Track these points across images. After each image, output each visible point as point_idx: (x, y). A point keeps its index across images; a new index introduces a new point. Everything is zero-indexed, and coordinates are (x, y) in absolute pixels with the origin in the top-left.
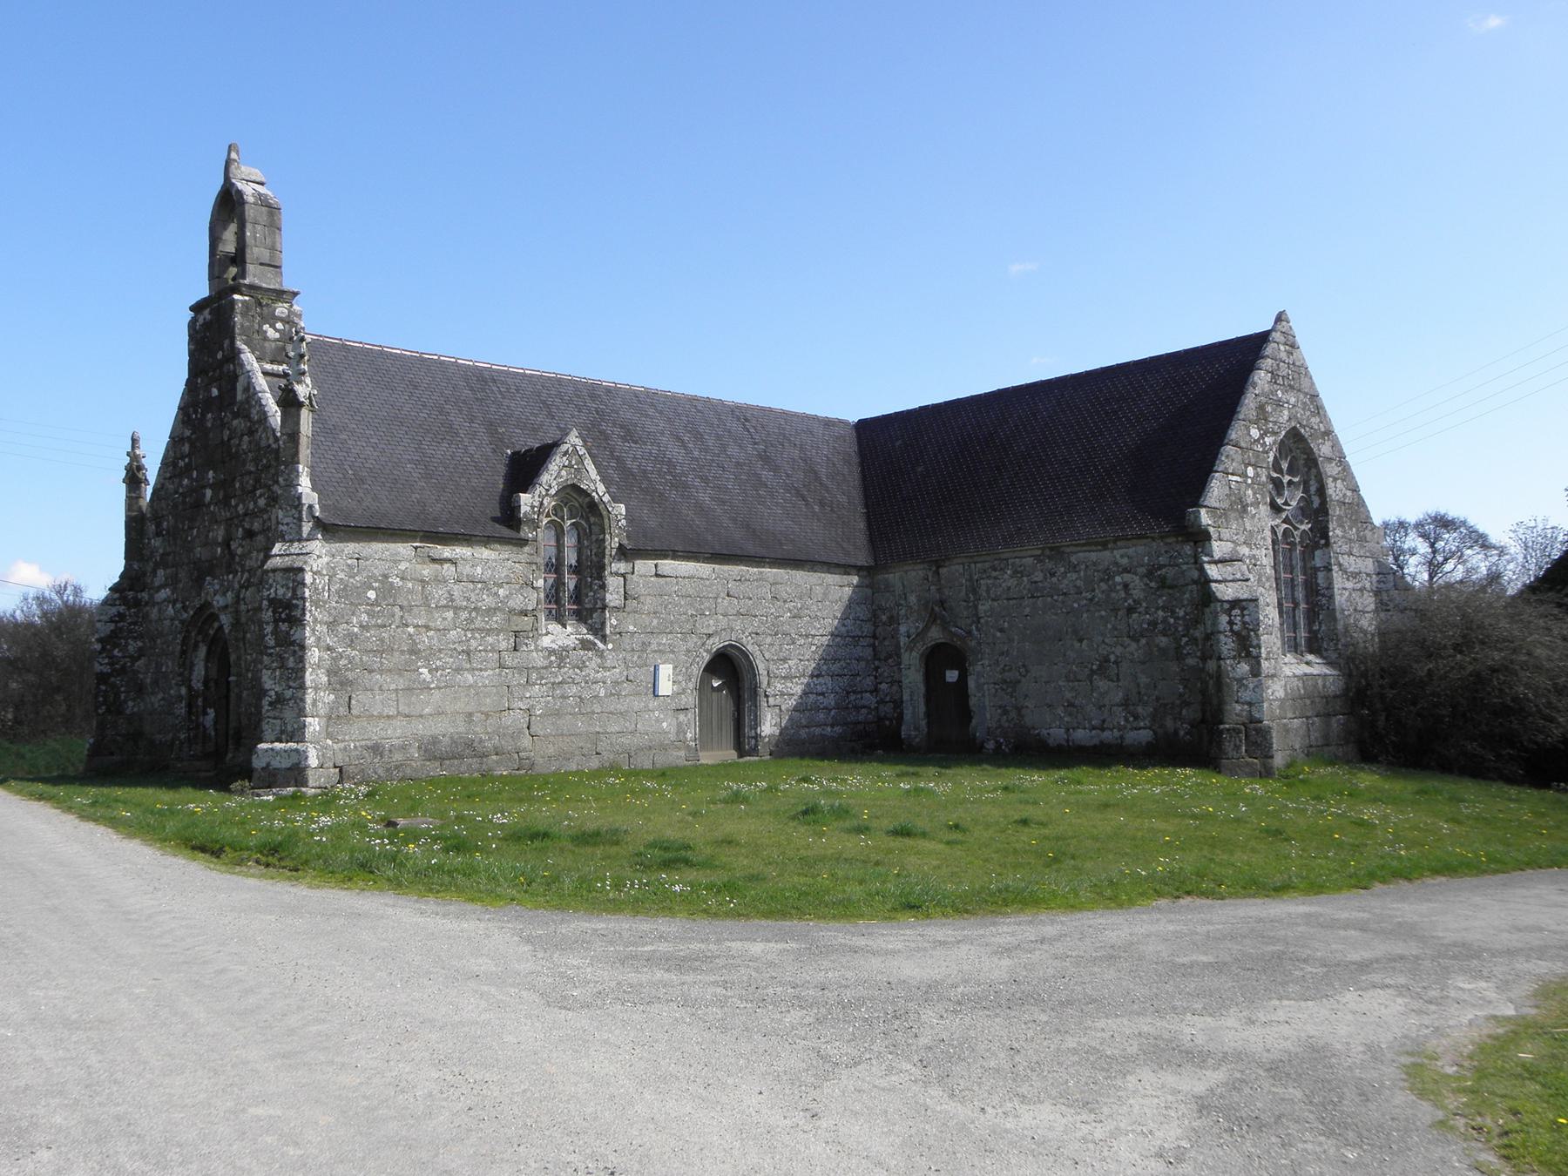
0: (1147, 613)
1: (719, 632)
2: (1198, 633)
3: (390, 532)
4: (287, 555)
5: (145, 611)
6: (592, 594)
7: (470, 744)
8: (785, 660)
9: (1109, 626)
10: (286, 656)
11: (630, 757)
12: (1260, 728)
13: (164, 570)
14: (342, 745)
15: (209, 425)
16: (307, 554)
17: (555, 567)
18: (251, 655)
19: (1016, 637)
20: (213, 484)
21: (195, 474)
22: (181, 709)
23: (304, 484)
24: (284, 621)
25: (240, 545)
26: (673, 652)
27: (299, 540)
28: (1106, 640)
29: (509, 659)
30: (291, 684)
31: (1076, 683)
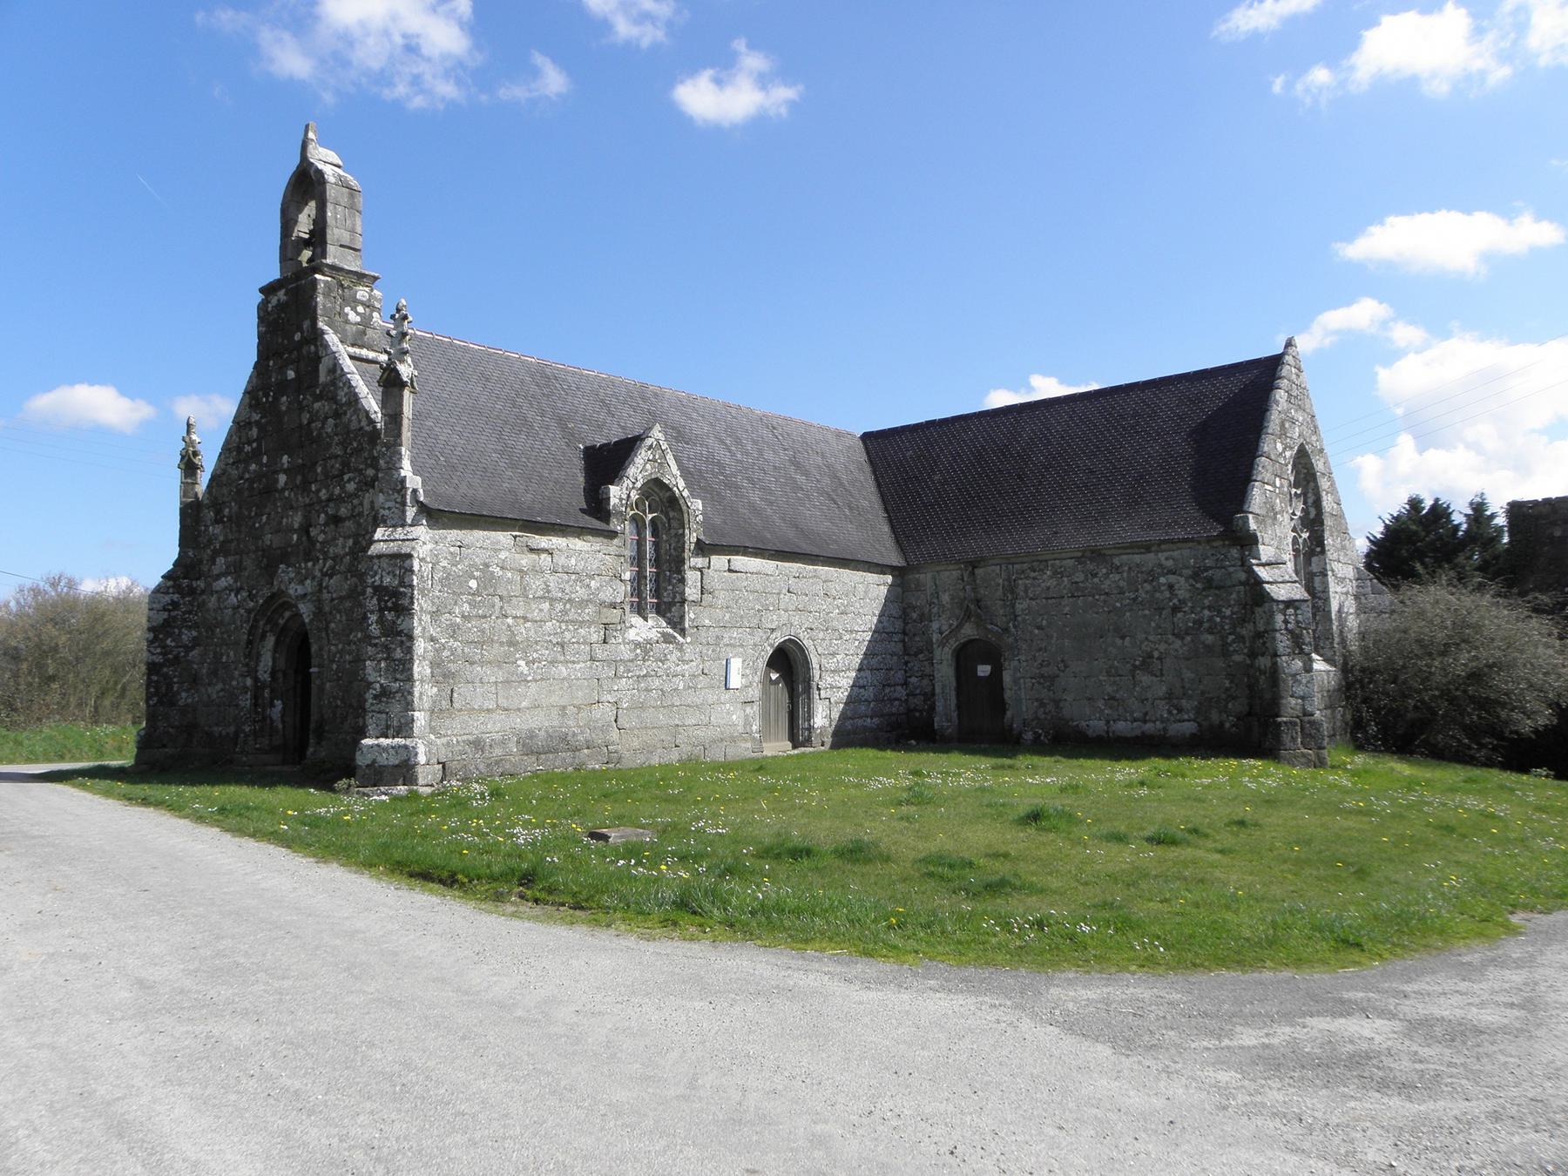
0: (1192, 612)
1: (782, 626)
2: (1247, 630)
3: (492, 520)
4: (391, 540)
5: (200, 600)
6: (671, 587)
7: (564, 738)
8: (834, 654)
9: (1153, 624)
10: (393, 646)
11: (705, 749)
12: (1314, 722)
13: (225, 557)
14: (444, 740)
15: (284, 408)
16: (413, 540)
17: (639, 560)
18: (336, 645)
19: (1055, 635)
20: (288, 469)
21: (265, 459)
22: (246, 701)
23: (406, 469)
24: (390, 610)
25: (322, 531)
26: (742, 646)
27: (403, 526)
28: (1151, 638)
29: (600, 652)
30: (398, 676)
31: (1118, 678)
